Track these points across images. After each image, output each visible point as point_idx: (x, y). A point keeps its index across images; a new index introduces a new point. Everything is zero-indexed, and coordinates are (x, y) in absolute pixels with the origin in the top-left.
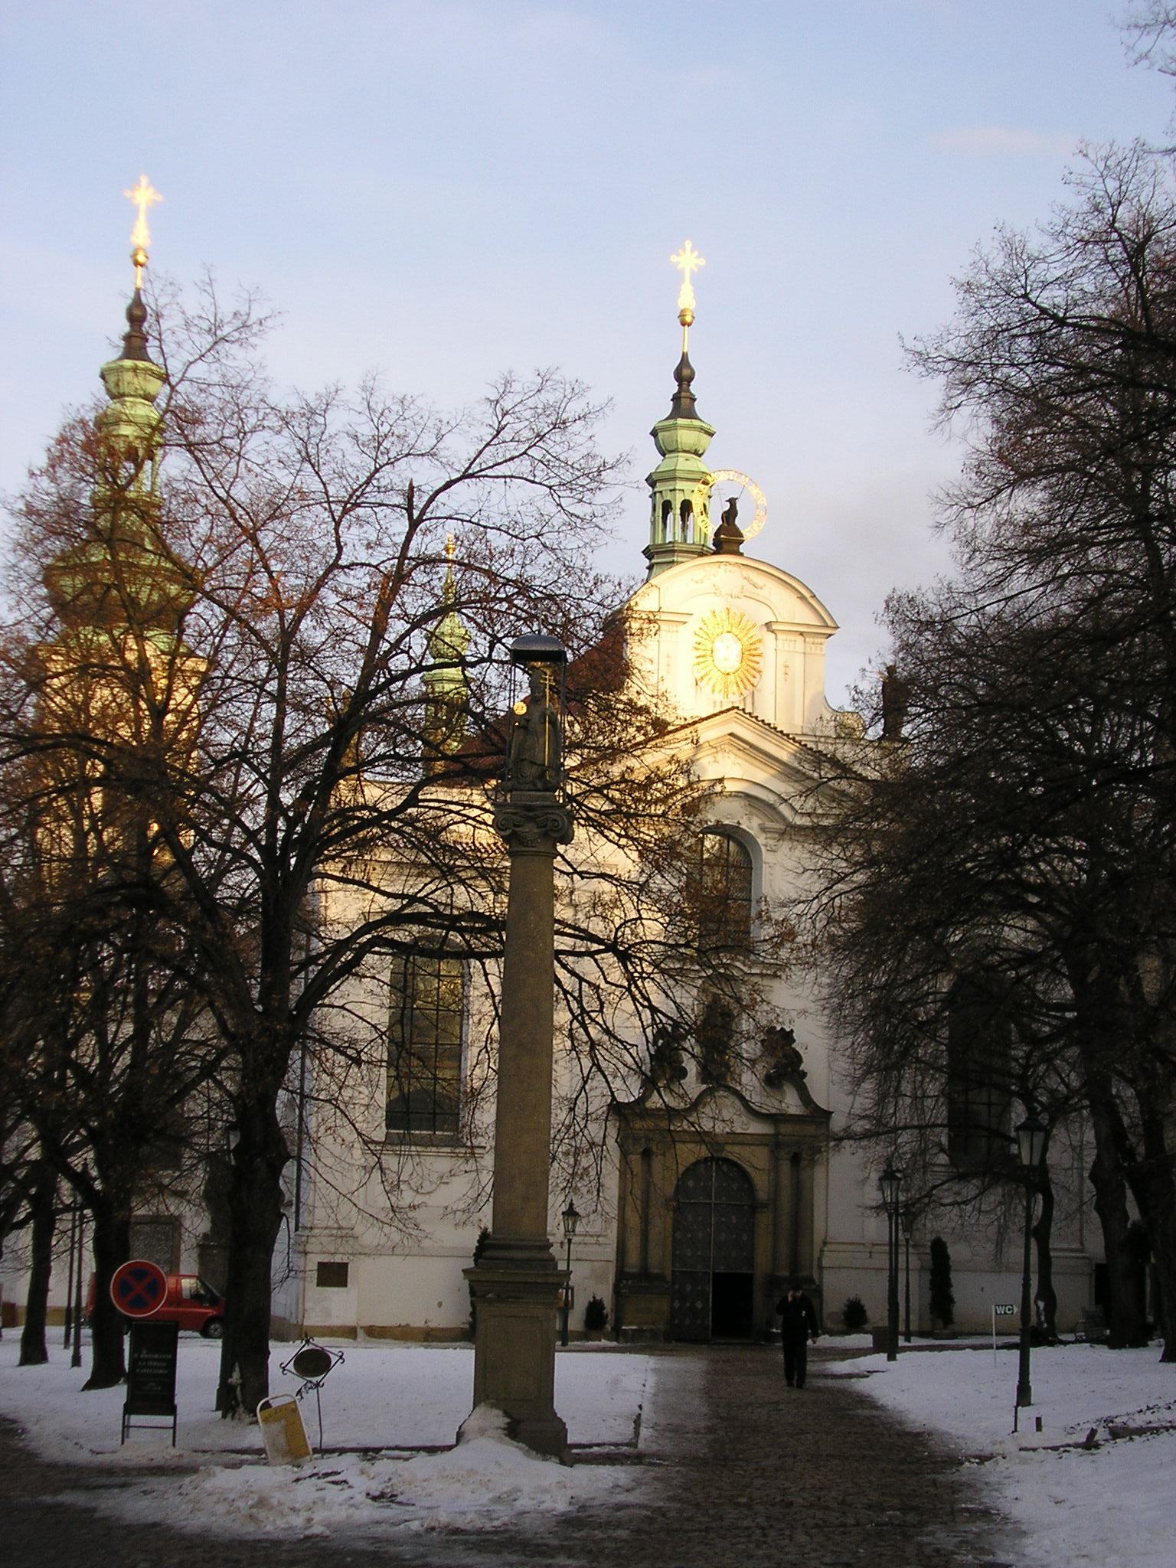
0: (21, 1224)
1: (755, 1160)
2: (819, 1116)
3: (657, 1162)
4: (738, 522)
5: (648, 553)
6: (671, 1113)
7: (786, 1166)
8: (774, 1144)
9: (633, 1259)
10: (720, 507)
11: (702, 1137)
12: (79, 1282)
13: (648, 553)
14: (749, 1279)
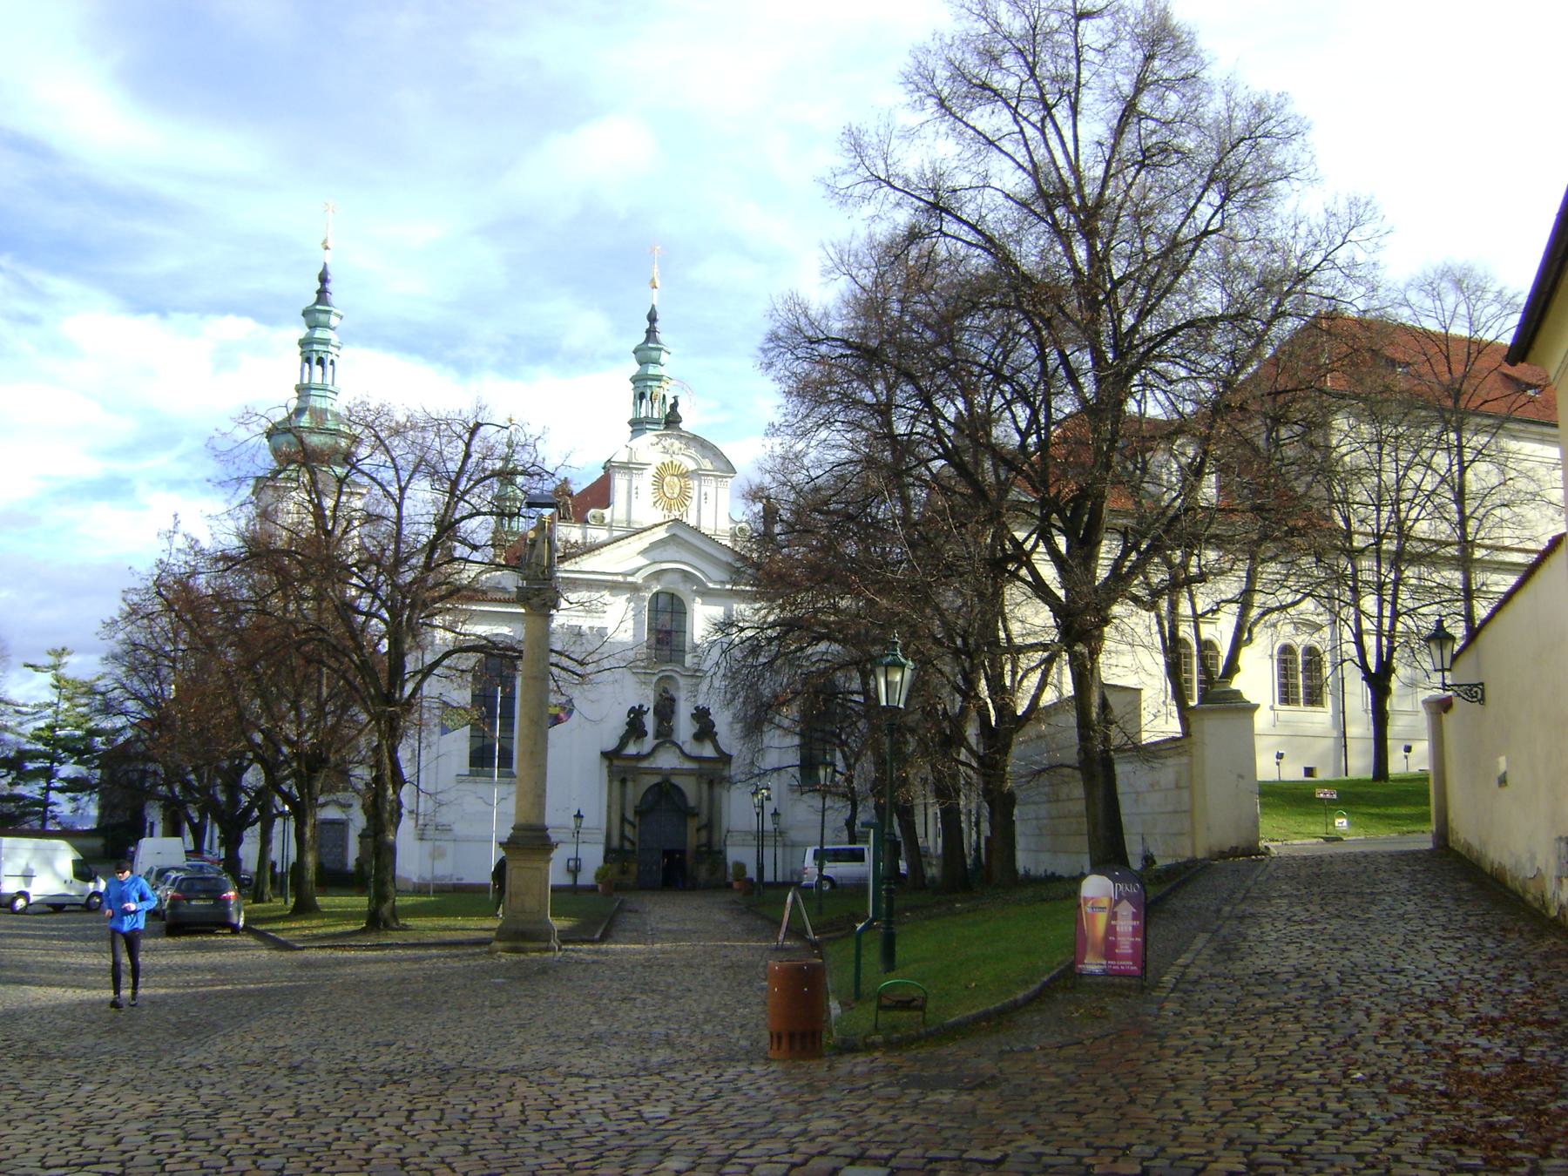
0: (253, 823)
1: (688, 786)
2: (725, 759)
3: (630, 785)
4: (679, 410)
5: (633, 423)
6: (639, 757)
7: (705, 787)
8: (698, 775)
9: (616, 842)
10: (670, 401)
11: (657, 771)
12: (18, 927)
13: (633, 423)
14: (683, 852)
